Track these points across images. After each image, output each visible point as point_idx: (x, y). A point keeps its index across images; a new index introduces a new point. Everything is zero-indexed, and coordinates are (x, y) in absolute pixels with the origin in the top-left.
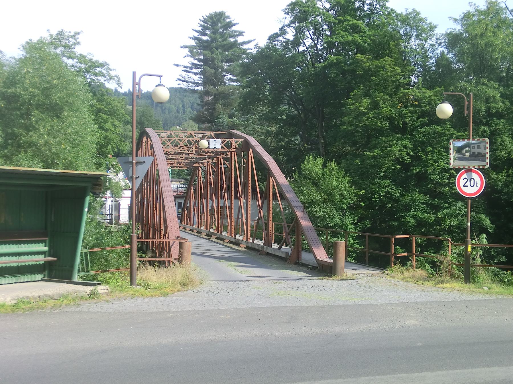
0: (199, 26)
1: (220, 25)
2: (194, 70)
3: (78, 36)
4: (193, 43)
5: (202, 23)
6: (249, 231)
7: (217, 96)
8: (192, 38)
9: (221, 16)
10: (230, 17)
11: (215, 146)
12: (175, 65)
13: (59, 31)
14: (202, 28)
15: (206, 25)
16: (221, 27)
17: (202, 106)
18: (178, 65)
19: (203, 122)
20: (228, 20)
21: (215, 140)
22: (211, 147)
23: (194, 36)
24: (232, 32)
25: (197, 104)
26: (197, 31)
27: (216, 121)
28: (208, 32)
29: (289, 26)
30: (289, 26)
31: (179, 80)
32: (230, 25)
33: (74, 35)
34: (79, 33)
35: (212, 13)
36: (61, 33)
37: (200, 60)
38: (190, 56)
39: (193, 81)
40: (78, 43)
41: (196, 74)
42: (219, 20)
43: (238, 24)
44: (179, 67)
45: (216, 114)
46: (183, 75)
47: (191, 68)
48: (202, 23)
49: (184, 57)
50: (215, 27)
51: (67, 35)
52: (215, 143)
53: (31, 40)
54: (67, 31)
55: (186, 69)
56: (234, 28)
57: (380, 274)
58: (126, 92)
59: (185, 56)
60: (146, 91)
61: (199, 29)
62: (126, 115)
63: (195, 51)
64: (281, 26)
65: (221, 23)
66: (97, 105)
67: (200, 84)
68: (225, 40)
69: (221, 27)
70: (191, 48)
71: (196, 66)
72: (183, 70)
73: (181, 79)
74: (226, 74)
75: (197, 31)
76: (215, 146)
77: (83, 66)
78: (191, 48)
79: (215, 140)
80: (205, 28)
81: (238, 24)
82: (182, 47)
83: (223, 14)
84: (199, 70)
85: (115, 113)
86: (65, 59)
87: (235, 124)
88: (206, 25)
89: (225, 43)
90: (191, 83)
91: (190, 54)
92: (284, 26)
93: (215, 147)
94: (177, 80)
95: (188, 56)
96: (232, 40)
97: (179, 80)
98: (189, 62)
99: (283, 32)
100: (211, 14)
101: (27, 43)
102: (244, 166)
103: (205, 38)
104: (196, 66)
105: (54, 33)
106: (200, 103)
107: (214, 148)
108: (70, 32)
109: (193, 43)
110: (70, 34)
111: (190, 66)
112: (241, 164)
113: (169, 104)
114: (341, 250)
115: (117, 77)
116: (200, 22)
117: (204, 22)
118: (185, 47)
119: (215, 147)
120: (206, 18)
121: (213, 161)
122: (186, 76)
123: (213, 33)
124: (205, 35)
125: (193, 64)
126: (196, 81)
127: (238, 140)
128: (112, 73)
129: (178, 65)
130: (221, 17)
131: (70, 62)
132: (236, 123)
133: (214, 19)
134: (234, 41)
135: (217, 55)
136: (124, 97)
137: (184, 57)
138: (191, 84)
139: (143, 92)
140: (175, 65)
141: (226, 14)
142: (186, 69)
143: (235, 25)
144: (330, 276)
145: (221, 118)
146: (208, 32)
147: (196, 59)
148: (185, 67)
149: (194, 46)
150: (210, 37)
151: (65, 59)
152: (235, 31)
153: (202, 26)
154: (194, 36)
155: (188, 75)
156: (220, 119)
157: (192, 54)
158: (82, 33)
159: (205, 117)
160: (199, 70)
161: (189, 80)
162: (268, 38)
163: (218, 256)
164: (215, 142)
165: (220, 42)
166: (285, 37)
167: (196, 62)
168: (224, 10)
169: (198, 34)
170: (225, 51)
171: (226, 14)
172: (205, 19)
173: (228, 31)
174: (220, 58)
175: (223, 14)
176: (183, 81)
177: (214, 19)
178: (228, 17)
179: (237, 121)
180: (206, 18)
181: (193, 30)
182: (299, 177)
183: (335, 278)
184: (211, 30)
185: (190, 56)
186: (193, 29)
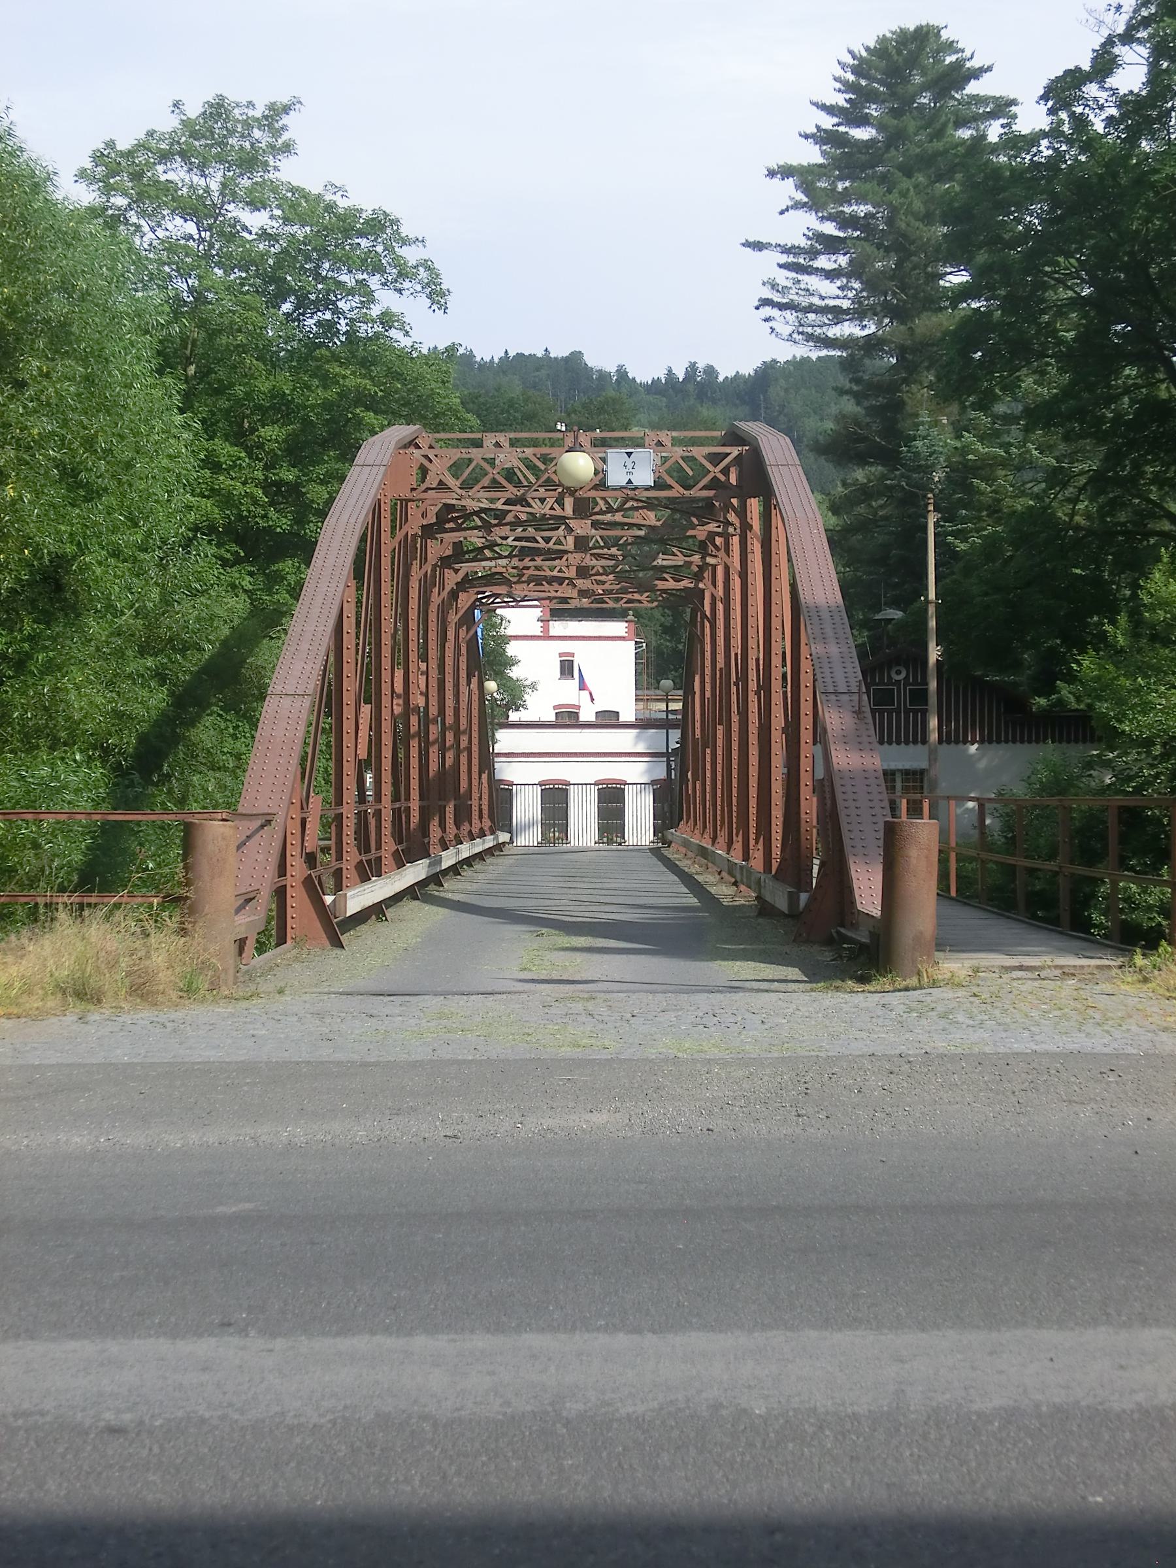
0: (839, 91)
1: (918, 79)
2: (823, 262)
3: (285, 120)
4: (812, 155)
5: (851, 77)
6: (773, 826)
7: (909, 357)
8: (813, 136)
9: (922, 42)
10: (960, 46)
11: (629, 477)
12: (748, 244)
13: (211, 106)
14: (848, 96)
15: (863, 83)
16: (924, 88)
17: (858, 397)
18: (758, 246)
19: (862, 460)
20: (950, 59)
21: (629, 454)
22: (611, 482)
23: (818, 127)
24: (969, 103)
25: (835, 389)
26: (830, 110)
27: (901, 452)
28: (873, 111)
29: (1127, 38)
30: (1127, 38)
31: (766, 302)
32: (961, 74)
33: (266, 117)
34: (286, 109)
35: (889, 35)
36: (218, 110)
37: (845, 222)
38: (804, 205)
39: (816, 301)
40: (287, 148)
41: (830, 275)
42: (913, 61)
43: (990, 69)
44: (765, 251)
45: (905, 425)
46: (778, 281)
47: (813, 254)
48: (851, 77)
49: (782, 213)
50: (900, 90)
51: (238, 117)
52: (630, 466)
53: (111, 144)
54: (238, 100)
55: (791, 259)
56: (973, 88)
57: (335, 865)
58: (656, 382)
59: (784, 207)
60: (731, 374)
61: (840, 100)
62: (469, 416)
63: (823, 184)
64: (1097, 42)
65: (923, 74)
66: (344, 377)
67: (846, 312)
68: (939, 134)
69: (924, 88)
70: (804, 176)
71: (830, 245)
72: (782, 262)
73: (775, 299)
74: (949, 270)
75: (830, 110)
76: (629, 477)
77: (300, 232)
78: (804, 176)
79: (629, 454)
80: (860, 95)
81: (990, 69)
82: (771, 174)
83: (928, 33)
84: (843, 260)
85: (426, 407)
86: (234, 211)
87: (970, 457)
88: (863, 83)
89: (938, 145)
90: (811, 309)
91: (805, 199)
92: (1110, 42)
93: (630, 482)
94: (757, 303)
95: (797, 205)
96: (965, 134)
97: (766, 302)
98: (806, 232)
99: (1104, 64)
100: (883, 40)
101: (98, 157)
102: (937, 604)
103: (862, 134)
104: (830, 245)
105: (194, 110)
106: (848, 386)
107: (624, 484)
108: (250, 104)
109: (812, 155)
110: (251, 113)
111: (804, 243)
112: (927, 597)
113: (817, 417)
114: (914, 861)
115: (428, 268)
116: (839, 72)
117: (856, 71)
118: (786, 172)
119: (630, 482)
120: (864, 54)
121: (703, 558)
122: (789, 284)
123: (895, 113)
124: (862, 121)
125: (820, 237)
126: (832, 303)
127: (727, 450)
128: (411, 255)
129: (758, 246)
130: (921, 48)
131: (256, 220)
132: (976, 451)
133: (896, 57)
134: (972, 137)
135: (904, 194)
136: (651, 398)
137: (782, 213)
138: (811, 316)
139: (721, 379)
140: (748, 244)
141: (944, 35)
142: (791, 259)
143: (977, 74)
144: (863, 980)
145: (924, 438)
146: (873, 111)
147: (830, 218)
148: (786, 250)
149: (821, 166)
150: (880, 127)
151: (234, 211)
152: (978, 100)
153: (848, 87)
154: (818, 127)
155: (799, 281)
156: (919, 443)
157: (815, 201)
158: (298, 106)
159: (864, 439)
160: (843, 260)
161: (805, 301)
162: (1042, 92)
163: (574, 919)
164: (629, 461)
165: (920, 144)
166: (1111, 82)
167: (830, 228)
168: (935, 21)
169: (836, 120)
170: (940, 178)
171: (944, 35)
172: (861, 59)
173: (952, 103)
174: (918, 205)
175: (928, 33)
176: (781, 307)
177: (896, 57)
178: (950, 47)
179: (979, 446)
180: (864, 54)
181: (816, 104)
182: (1135, 635)
183: (883, 982)
184: (883, 102)
185: (804, 205)
186: (815, 100)
